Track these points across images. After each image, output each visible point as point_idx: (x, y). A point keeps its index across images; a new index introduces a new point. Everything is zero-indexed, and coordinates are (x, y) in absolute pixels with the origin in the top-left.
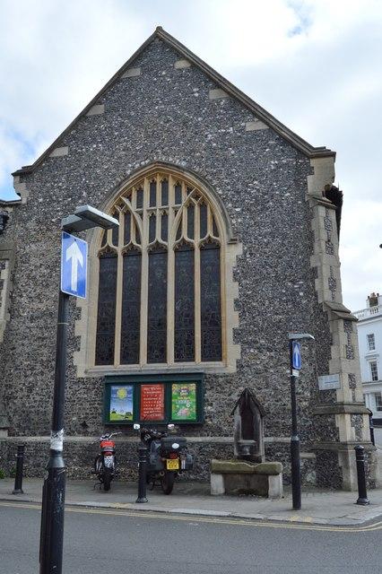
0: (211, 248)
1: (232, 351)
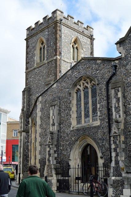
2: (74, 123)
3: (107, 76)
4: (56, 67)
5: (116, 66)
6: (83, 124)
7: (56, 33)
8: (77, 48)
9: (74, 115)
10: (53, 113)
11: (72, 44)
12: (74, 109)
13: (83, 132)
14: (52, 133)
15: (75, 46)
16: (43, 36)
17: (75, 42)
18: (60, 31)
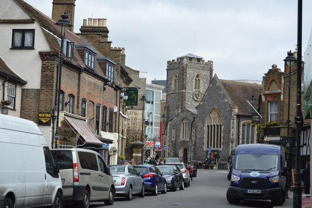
0: (221, 126)
1: (222, 146)
2: (181, 138)
3: (192, 120)
4: (182, 97)
5: (194, 118)
6: (184, 139)
7: (183, 75)
8: (199, 80)
9: (181, 134)
10: (173, 132)
11: (195, 78)
12: (182, 131)
13: (184, 142)
14: (172, 142)
15: (197, 79)
16: (177, 72)
17: (198, 76)
18: (186, 72)
